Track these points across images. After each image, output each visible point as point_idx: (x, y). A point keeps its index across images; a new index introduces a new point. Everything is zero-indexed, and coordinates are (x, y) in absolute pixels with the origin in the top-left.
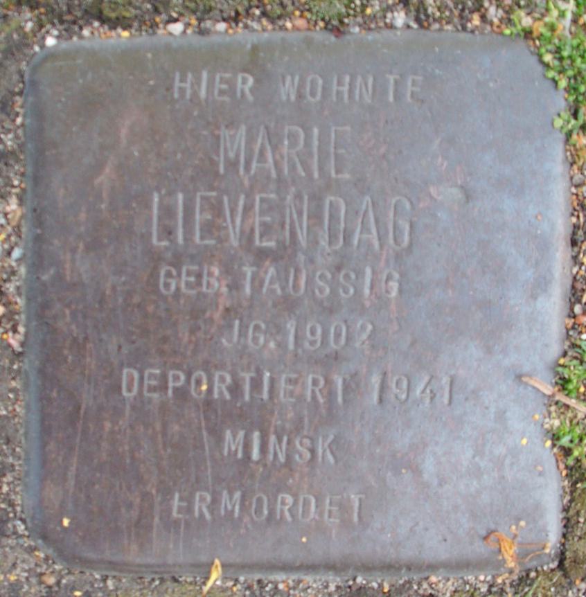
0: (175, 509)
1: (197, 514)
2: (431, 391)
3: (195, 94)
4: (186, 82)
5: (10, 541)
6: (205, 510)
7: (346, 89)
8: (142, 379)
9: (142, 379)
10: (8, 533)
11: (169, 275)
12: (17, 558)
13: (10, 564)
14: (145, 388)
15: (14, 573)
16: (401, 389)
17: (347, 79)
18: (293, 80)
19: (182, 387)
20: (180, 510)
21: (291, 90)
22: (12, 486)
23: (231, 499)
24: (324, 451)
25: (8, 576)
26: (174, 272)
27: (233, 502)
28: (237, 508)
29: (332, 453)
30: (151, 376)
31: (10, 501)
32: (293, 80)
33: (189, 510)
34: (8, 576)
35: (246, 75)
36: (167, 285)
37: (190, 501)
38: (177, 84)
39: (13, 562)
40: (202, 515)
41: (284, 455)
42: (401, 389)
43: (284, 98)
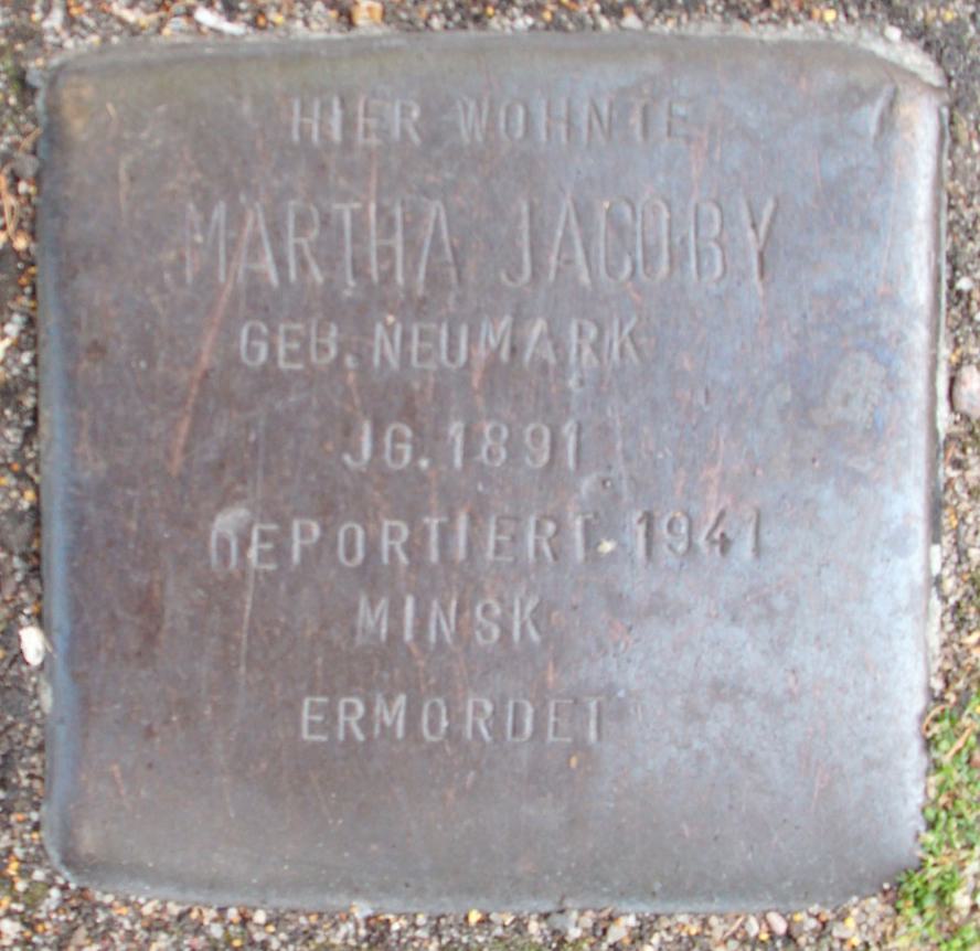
0: (305, 727)
1: (341, 736)
3: (324, 136)
4: (311, 116)
6: (411, 131)
11: (253, 334)
15: (951, 6)
16: (675, 535)
20: (313, 727)
21: (477, 127)
24: (523, 627)
25: (942, 11)
26: (264, 329)
27: (394, 712)
28: (400, 724)
34: (942, 11)
36: (252, 352)
37: (332, 714)
38: (296, 119)
41: (453, 628)
42: (675, 535)
43: (467, 140)
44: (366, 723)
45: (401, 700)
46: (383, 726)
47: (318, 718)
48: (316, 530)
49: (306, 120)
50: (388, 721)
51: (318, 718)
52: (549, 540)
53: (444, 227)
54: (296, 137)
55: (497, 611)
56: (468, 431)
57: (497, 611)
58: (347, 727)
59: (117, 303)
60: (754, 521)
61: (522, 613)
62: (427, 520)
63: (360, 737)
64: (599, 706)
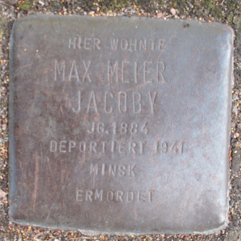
2: (176, 148)
3: (77, 48)
4: (135, 43)
5: (237, 228)
7: (135, 45)
8: (58, 145)
9: (58, 145)
10: (237, 225)
12: (239, 235)
13: (236, 237)
14: (60, 148)
17: (136, 41)
18: (116, 41)
19: (75, 148)
20: (79, 198)
22: (239, 206)
23: (99, 193)
29: (134, 171)
30: (63, 144)
31: (238, 212)
32: (116, 41)
33: (84, 197)
35: (97, 39)
39: (237, 236)
40: (119, 199)
44: (93, 197)
45: (102, 191)
46: (97, 197)
47: (80, 195)
48: (75, 144)
49: (133, 44)
50: (98, 196)
51: (80, 195)
52: (134, 149)
53: (85, 64)
54: (70, 47)
55: (124, 168)
56: (117, 125)
57: (124, 168)
58: (88, 197)
59: (69, 212)
60: (182, 144)
61: (131, 168)
62: (102, 142)
63: (91, 200)
64: (106, 144)
